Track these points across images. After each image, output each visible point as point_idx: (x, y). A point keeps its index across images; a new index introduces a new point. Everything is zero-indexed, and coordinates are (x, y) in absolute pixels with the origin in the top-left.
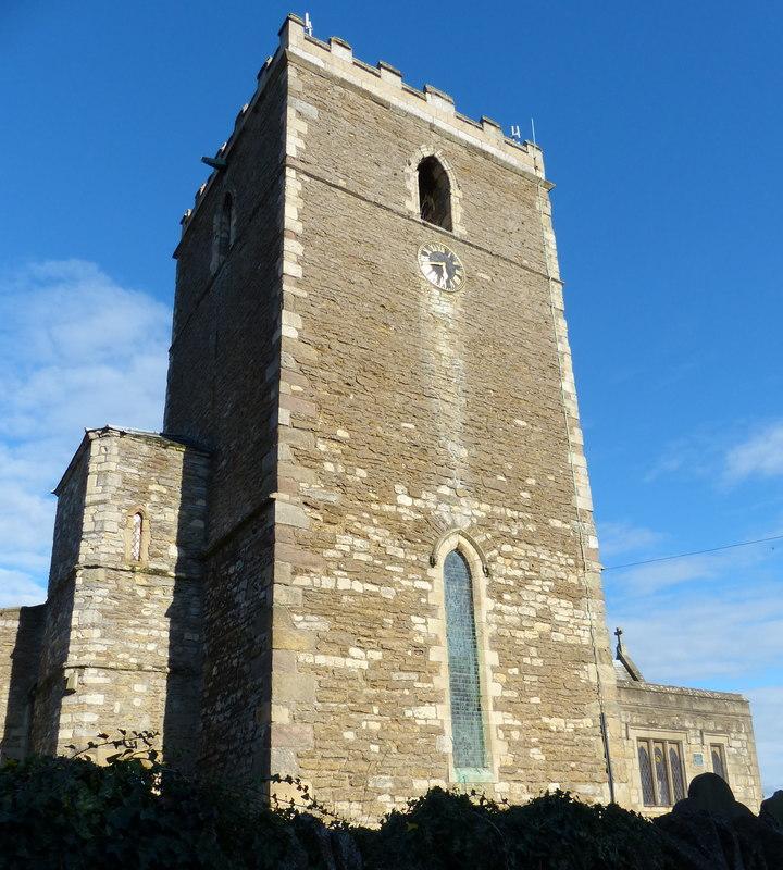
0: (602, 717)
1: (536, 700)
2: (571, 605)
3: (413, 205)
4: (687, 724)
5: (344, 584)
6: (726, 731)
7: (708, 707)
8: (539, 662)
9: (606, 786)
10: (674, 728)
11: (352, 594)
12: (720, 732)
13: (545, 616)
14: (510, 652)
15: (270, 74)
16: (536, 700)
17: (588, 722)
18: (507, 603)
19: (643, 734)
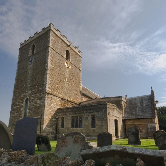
0: (41, 115)
1: (33, 115)
2: (40, 100)
3: (65, 56)
4: (84, 112)
5: (16, 107)
6: (97, 111)
7: (92, 107)
8: (34, 110)
9: (40, 126)
10: (81, 113)
11: (16, 108)
12: (95, 112)
13: (36, 103)
14: (30, 109)
15: (144, 53)
16: (33, 115)
17: (39, 117)
18: (31, 103)
19: (73, 115)
